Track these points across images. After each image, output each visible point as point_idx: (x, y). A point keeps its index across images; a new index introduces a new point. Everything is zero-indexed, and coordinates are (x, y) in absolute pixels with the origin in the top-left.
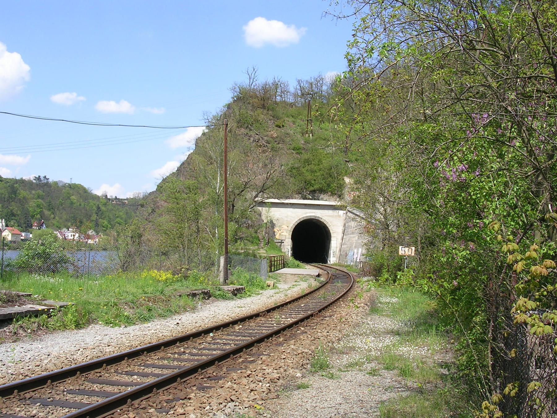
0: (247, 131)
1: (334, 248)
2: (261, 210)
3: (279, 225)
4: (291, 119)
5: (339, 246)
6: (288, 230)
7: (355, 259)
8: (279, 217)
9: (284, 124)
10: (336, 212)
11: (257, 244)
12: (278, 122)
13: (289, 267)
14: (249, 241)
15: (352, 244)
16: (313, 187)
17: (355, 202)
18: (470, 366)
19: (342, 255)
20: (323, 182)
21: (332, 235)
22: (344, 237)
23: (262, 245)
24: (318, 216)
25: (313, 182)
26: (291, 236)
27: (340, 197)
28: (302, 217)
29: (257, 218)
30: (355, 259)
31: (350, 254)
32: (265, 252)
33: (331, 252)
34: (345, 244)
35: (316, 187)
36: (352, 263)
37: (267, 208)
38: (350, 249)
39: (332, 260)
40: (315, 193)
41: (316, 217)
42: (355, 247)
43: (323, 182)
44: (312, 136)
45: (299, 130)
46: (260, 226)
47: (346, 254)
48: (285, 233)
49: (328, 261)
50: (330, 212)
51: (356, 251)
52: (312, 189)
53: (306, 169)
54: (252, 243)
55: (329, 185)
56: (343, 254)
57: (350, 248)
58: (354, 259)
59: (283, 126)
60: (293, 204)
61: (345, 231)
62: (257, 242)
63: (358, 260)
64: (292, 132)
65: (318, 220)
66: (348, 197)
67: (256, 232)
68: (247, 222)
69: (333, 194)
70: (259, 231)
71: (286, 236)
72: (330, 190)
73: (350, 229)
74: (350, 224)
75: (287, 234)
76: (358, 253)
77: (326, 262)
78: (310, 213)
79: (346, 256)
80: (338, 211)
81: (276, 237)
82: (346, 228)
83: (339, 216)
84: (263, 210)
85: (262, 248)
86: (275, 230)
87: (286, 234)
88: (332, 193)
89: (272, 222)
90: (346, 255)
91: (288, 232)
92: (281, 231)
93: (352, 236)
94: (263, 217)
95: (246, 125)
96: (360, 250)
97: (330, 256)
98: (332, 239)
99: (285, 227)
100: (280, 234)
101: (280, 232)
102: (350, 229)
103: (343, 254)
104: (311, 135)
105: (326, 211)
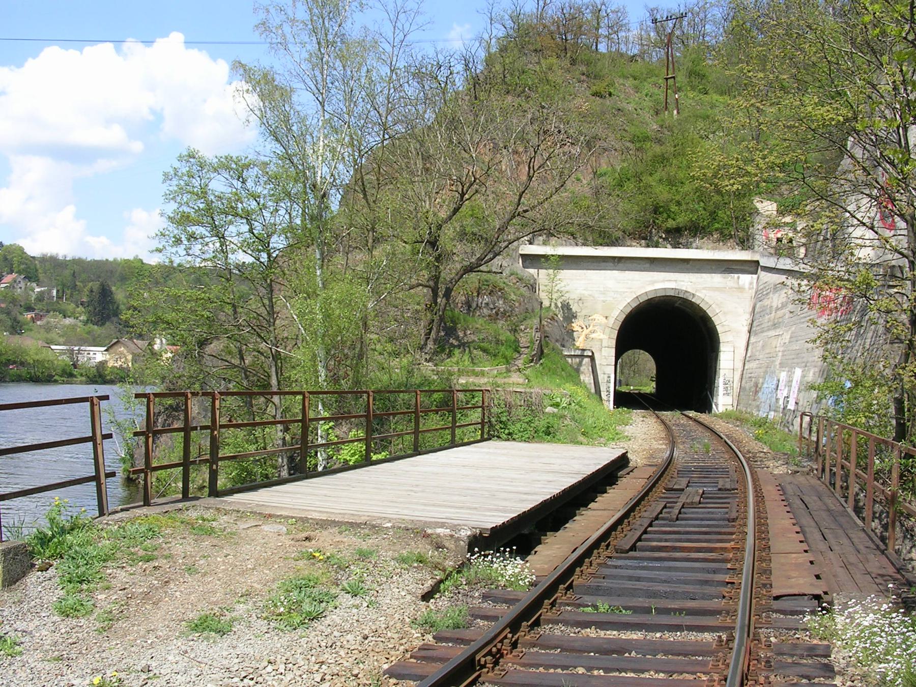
0: (521, 100)
1: (726, 372)
2: (536, 277)
3: (584, 312)
4: (630, 82)
5: (739, 365)
6: (606, 326)
7: (781, 402)
8: (584, 292)
9: (611, 90)
10: (730, 280)
11: (507, 361)
12: (599, 86)
13: (510, 437)
14: (485, 350)
15: (771, 357)
16: (674, 220)
17: (783, 248)
18: (495, 129)
19: (745, 388)
20: (699, 207)
21: (722, 337)
22: (753, 340)
23: (520, 363)
24: (684, 289)
25: (674, 208)
26: (614, 342)
27: (745, 243)
28: (643, 291)
29: (522, 295)
30: (781, 402)
31: (769, 385)
32: (521, 381)
33: (720, 382)
34: (753, 358)
35: (682, 220)
36: (772, 415)
37: (551, 271)
38: (766, 372)
39: (723, 401)
40: (681, 236)
41: (679, 291)
42: (782, 365)
43: (699, 207)
44: (678, 113)
45: (648, 103)
46: (528, 313)
47: (756, 385)
48: (598, 335)
49: (714, 406)
50: (716, 279)
51: (783, 376)
52: (671, 224)
53: (657, 176)
54: (495, 356)
55: (713, 216)
56: (747, 386)
57: (768, 370)
58: (777, 400)
59: (610, 94)
60: (620, 259)
61: (755, 324)
62: (509, 353)
63: (791, 406)
64: (630, 107)
65: (685, 301)
66: (764, 236)
67: (515, 331)
68: (494, 304)
69: (725, 237)
70: (522, 327)
71: (601, 340)
72: (717, 225)
73: (767, 317)
74: (766, 302)
75: (604, 337)
76: (789, 383)
77: (704, 403)
78: (663, 281)
79: (756, 392)
80: (736, 275)
81: (577, 344)
82: (757, 316)
83: (741, 289)
84: (542, 276)
85: (519, 370)
86: (576, 326)
87: (602, 336)
88: (721, 233)
89: (566, 307)
90: (757, 389)
91: (608, 330)
92: (591, 328)
93: (772, 333)
94: (543, 296)
95: (519, 90)
96: (798, 372)
97: (717, 391)
98: (723, 348)
99: (599, 318)
100: (587, 337)
101: (586, 331)
102: (767, 317)
103: (747, 386)
104: (675, 112)
105: (704, 275)
